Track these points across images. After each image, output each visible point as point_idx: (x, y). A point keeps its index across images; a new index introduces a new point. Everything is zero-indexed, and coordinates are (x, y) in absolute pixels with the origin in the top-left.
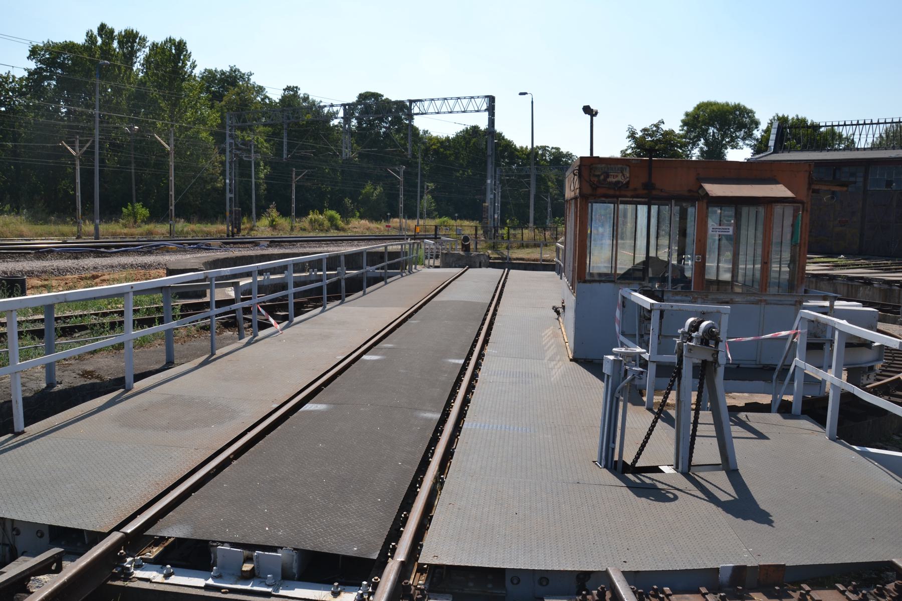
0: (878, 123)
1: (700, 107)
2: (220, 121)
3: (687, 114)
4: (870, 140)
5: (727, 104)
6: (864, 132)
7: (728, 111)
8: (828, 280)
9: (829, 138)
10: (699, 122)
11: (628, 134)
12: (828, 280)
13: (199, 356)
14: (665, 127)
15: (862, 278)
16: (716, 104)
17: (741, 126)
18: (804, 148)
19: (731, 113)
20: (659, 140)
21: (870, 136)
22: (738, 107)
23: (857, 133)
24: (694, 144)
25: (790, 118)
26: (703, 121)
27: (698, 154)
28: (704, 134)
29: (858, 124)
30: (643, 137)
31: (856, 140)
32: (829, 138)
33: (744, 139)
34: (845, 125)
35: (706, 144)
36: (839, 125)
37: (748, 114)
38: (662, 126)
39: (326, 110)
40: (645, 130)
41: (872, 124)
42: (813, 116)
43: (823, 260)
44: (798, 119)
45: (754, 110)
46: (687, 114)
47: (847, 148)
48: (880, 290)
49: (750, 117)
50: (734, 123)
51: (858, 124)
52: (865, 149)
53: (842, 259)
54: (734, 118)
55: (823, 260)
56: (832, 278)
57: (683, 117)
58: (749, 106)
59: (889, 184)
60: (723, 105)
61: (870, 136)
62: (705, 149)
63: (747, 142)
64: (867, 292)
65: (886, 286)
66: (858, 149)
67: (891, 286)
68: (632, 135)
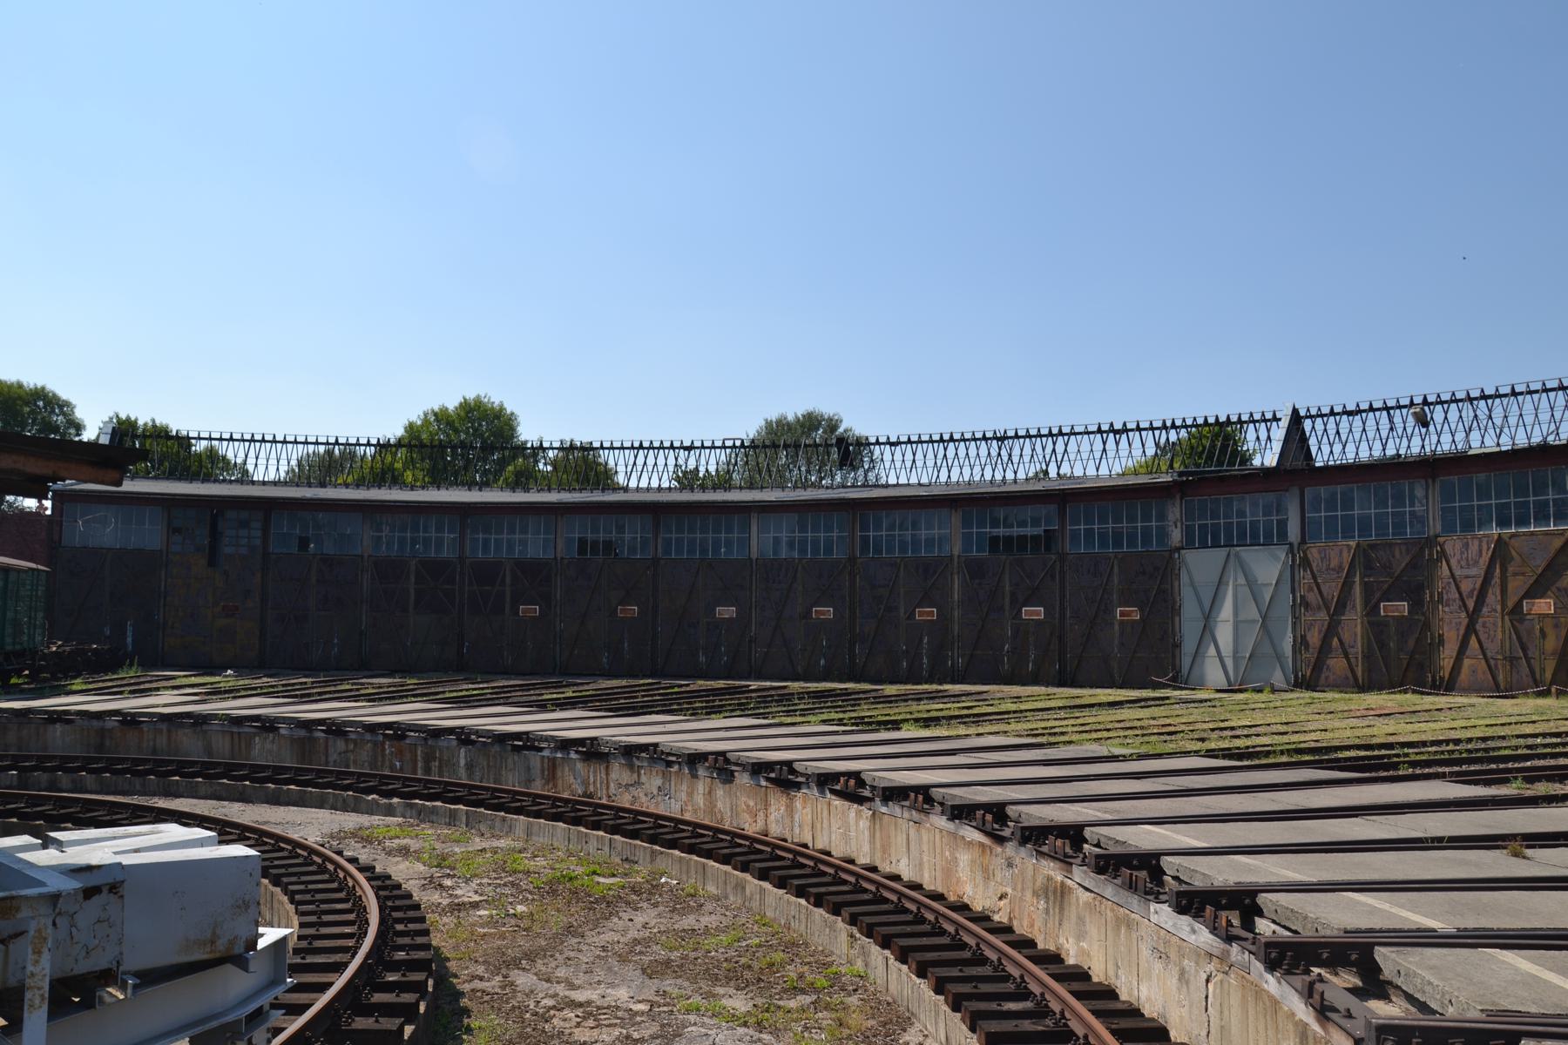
0: (285, 442)
4: (283, 468)
5: (20, 386)
6: (262, 455)
7: (20, 398)
13: (1358, 902)
15: (188, 715)
19: (27, 404)
21: (283, 462)
22: (40, 394)
23: (252, 454)
25: (141, 423)
29: (252, 440)
31: (250, 468)
34: (231, 439)
36: (221, 439)
37: (61, 407)
39: (200, 447)
41: (274, 441)
42: (178, 422)
43: (194, 680)
44: (154, 426)
45: (74, 402)
47: (240, 481)
48: (293, 740)
49: (64, 414)
50: (34, 423)
51: (252, 440)
52: (264, 483)
53: (228, 679)
54: (32, 412)
55: (194, 680)
56: (200, 720)
58: (64, 394)
59: (303, 543)
60: (11, 386)
61: (283, 462)
64: (268, 746)
65: (302, 733)
66: (253, 482)
67: (311, 731)
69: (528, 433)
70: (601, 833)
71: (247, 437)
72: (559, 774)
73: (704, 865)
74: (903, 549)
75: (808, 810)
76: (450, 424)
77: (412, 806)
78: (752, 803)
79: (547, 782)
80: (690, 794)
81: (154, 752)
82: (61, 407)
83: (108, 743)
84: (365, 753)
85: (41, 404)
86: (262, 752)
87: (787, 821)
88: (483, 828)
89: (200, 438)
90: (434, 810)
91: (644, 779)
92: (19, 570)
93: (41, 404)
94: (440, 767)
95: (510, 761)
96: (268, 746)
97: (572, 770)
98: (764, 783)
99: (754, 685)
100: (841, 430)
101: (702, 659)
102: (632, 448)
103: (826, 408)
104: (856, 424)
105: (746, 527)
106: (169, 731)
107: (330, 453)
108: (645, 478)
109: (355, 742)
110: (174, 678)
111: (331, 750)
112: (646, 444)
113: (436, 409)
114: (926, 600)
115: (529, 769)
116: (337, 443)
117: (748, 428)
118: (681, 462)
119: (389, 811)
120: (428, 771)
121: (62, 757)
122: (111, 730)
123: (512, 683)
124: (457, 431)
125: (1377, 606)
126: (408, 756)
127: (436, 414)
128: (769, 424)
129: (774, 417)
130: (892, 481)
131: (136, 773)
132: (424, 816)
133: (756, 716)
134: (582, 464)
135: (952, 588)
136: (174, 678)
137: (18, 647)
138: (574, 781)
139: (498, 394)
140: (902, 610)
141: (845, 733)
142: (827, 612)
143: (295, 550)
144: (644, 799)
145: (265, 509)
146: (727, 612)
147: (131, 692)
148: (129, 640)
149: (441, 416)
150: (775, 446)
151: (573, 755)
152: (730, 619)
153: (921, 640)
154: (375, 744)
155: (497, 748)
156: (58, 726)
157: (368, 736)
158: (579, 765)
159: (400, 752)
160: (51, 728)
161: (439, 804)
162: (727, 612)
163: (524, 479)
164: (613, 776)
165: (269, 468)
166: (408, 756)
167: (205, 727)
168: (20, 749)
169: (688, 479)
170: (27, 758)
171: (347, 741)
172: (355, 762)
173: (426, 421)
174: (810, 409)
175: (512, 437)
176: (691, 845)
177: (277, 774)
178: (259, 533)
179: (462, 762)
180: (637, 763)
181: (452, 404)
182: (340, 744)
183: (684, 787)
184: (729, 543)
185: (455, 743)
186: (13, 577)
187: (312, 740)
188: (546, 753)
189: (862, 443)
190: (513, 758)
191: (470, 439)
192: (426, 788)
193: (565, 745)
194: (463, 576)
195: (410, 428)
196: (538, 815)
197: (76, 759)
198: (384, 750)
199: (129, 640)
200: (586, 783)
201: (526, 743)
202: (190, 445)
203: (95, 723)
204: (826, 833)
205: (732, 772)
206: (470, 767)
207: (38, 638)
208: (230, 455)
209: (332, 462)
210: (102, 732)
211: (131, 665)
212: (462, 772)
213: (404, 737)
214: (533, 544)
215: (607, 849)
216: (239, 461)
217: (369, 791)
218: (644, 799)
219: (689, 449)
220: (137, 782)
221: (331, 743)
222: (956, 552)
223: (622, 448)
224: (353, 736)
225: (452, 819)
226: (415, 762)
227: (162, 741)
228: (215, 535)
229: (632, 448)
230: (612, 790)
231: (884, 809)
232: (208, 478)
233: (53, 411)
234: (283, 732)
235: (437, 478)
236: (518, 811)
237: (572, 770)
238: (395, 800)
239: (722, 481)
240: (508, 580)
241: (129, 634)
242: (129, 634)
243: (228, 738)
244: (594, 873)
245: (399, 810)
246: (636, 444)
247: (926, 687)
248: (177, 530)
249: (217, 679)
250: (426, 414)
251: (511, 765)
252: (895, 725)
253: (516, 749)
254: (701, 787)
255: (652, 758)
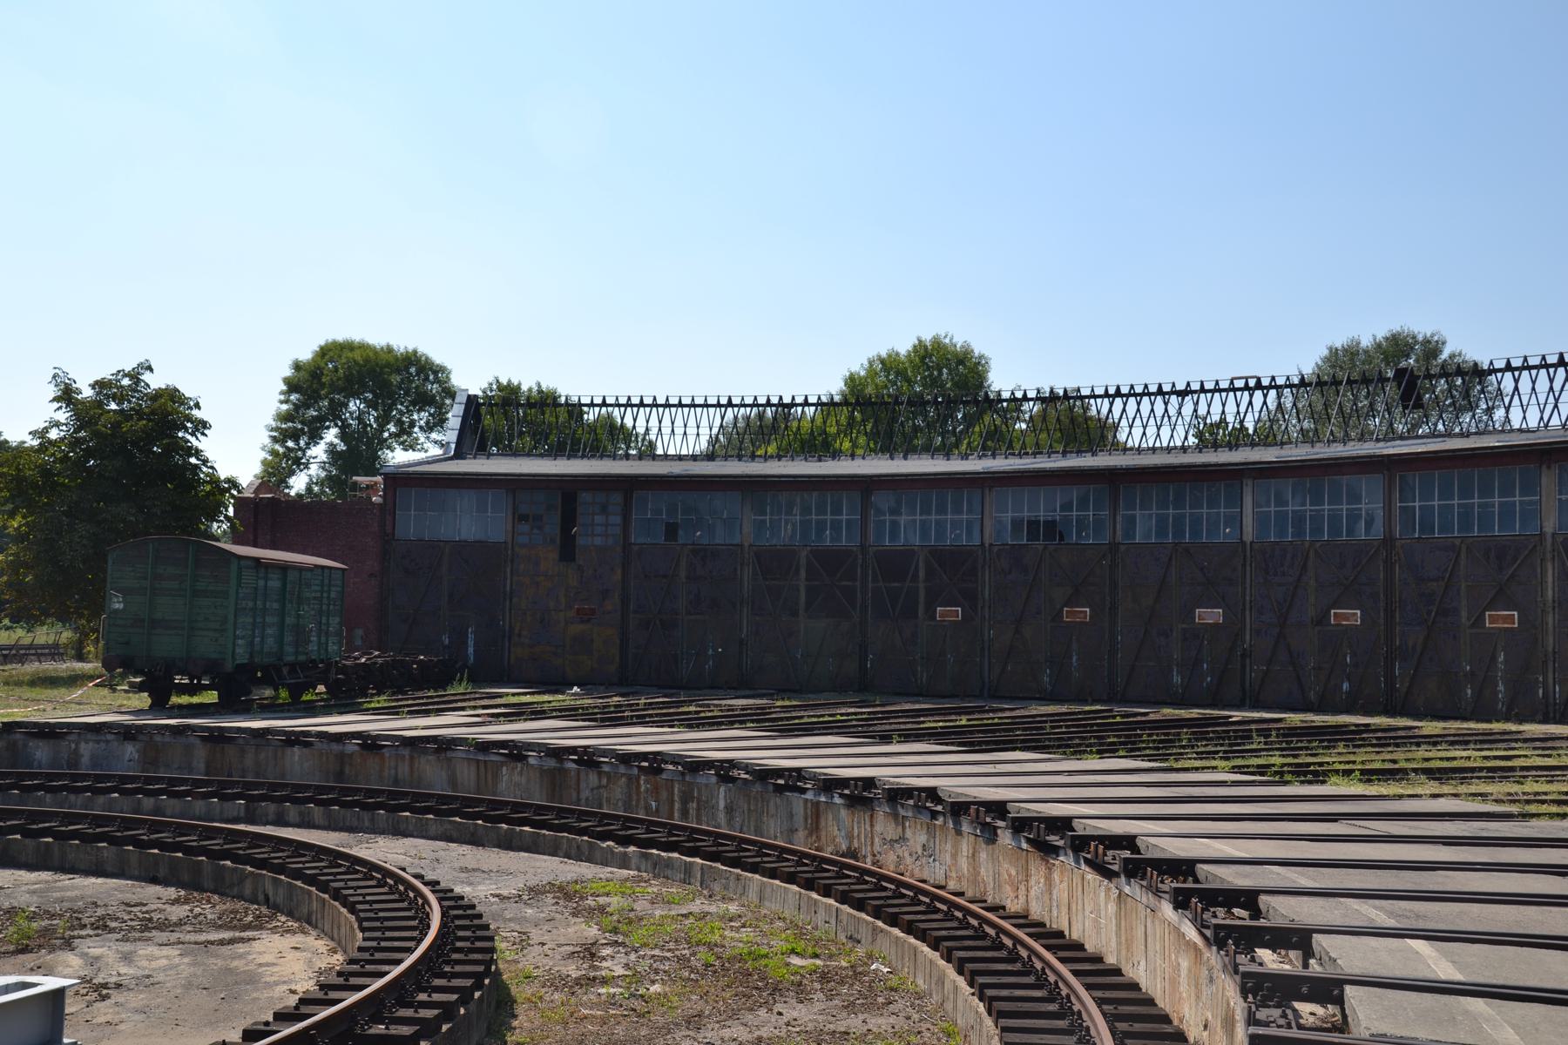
1: (326, 352)
2: (660, 451)
3: (297, 366)
5: (390, 350)
7: (388, 365)
8: (437, 751)
9: (604, 437)
10: (323, 385)
11: (52, 391)
12: (437, 751)
14: (154, 381)
15: (434, 739)
16: (363, 347)
17: (423, 401)
18: (557, 451)
19: (398, 371)
20: (139, 412)
21: (704, 431)
24: (315, 437)
25: (524, 388)
26: (332, 384)
27: (324, 457)
28: (334, 413)
30: (98, 404)
32: (604, 437)
33: (428, 428)
35: (343, 436)
37: (436, 373)
38: (146, 377)
39: (591, 416)
40: (100, 385)
41: (694, 405)
42: (570, 387)
44: (540, 391)
46: (297, 366)
48: (542, 771)
50: (407, 393)
57: (288, 372)
58: (438, 359)
59: (671, 531)
62: (342, 447)
63: (434, 435)
64: (516, 778)
65: (551, 763)
66: (1125, 449)
67: (561, 761)
68: (67, 395)
69: (1001, 381)
70: (831, 901)
71: (686, 401)
72: (823, 823)
73: (915, 949)
74: (1466, 524)
75: (1065, 884)
76: (901, 373)
77: (646, 856)
78: (1013, 873)
79: (810, 834)
80: (954, 856)
81: (396, 782)
82: (436, 373)
83: (347, 770)
84: (618, 790)
85: (413, 370)
86: (512, 785)
87: (1046, 897)
88: (717, 887)
89: (592, 405)
90: (669, 864)
91: (909, 833)
92: (300, 569)
93: (413, 370)
94: (698, 809)
95: (772, 804)
96: (516, 778)
97: (836, 818)
98: (1025, 846)
99: (1237, 715)
100: (1444, 356)
101: (1177, 679)
102: (719, 405)
103: (1421, 327)
104: (1468, 342)
105: (1530, 487)
106: (412, 758)
107: (761, 416)
108: (1150, 434)
109: (608, 774)
110: (500, 696)
111: (583, 785)
112: (1125, 390)
113: (884, 354)
114: (1502, 598)
115: (791, 816)
116: (769, 404)
117: (1305, 360)
118: (1202, 411)
119: (624, 863)
120: (685, 814)
121: (317, 787)
122: (351, 755)
123: (917, 706)
124: (909, 381)
125: (1481, 618)
126: (664, 795)
127: (882, 362)
128: (1334, 352)
129: (1340, 342)
130: (1134, 441)
131: (365, 807)
132: (660, 870)
133: (1151, 758)
134: (1068, 418)
135: (1543, 582)
136: (500, 696)
137: (302, 658)
138: (841, 831)
139: (961, 332)
140: (1464, 614)
141: (1262, 783)
142: (1352, 616)
143: (662, 540)
144: (909, 860)
145: (683, 488)
146: (1211, 615)
147: (410, 712)
148: (471, 650)
149: (889, 365)
150: (1336, 382)
151: (837, 800)
152: (1216, 625)
153: (1494, 658)
154: (630, 778)
155: (758, 787)
156: (296, 749)
157: (622, 769)
158: (844, 813)
159: (655, 791)
160: (289, 751)
161: (676, 855)
162: (1211, 615)
163: (997, 441)
164: (878, 828)
165: (683, 440)
166: (664, 795)
167: (450, 754)
168: (257, 775)
169: (1210, 435)
170: (257, 785)
171: (600, 774)
172: (608, 800)
173: (871, 372)
174: (1396, 328)
175: (981, 386)
176: (910, 922)
177: (516, 812)
178: (618, 519)
179: (722, 804)
180: (902, 812)
181: (904, 347)
182: (593, 778)
183: (949, 847)
184: (836, 526)
185: (714, 780)
186: (292, 576)
187: (563, 772)
188: (809, 796)
189: (1478, 373)
190: (775, 800)
191: (930, 392)
192: (648, 831)
193: (831, 785)
194: (935, 568)
195: (852, 380)
196: (773, 874)
197: (307, 787)
198: (639, 786)
199: (471, 650)
200: (850, 837)
201: (793, 780)
202: (581, 413)
203: (335, 747)
204: (1080, 917)
205: (996, 828)
206: (729, 810)
207: (332, 648)
208: (629, 422)
209: (770, 426)
210: (342, 758)
211: (461, 680)
212: (722, 817)
213: (660, 771)
214: (957, 528)
215: (833, 921)
216: (641, 430)
217: (604, 836)
218: (909, 860)
219: (1182, 394)
220: (366, 816)
221: (583, 775)
222: (1550, 526)
223: (706, 405)
224: (606, 768)
225: (687, 874)
226: (672, 802)
227: (404, 770)
228: (569, 519)
229: (719, 405)
230: (877, 848)
231: (1127, 889)
232: (596, 450)
233: (427, 379)
234: (532, 761)
235: (887, 444)
236: (754, 869)
237: (836, 818)
238: (632, 849)
239: (1267, 435)
240: (922, 574)
241: (471, 643)
242: (471, 643)
243: (473, 768)
244: (793, 951)
245: (634, 861)
246: (724, 401)
247: (1472, 725)
248: (523, 518)
249: (561, 697)
250: (871, 363)
251: (772, 810)
252: (1319, 776)
253: (779, 789)
254: (965, 846)
255: (916, 806)
